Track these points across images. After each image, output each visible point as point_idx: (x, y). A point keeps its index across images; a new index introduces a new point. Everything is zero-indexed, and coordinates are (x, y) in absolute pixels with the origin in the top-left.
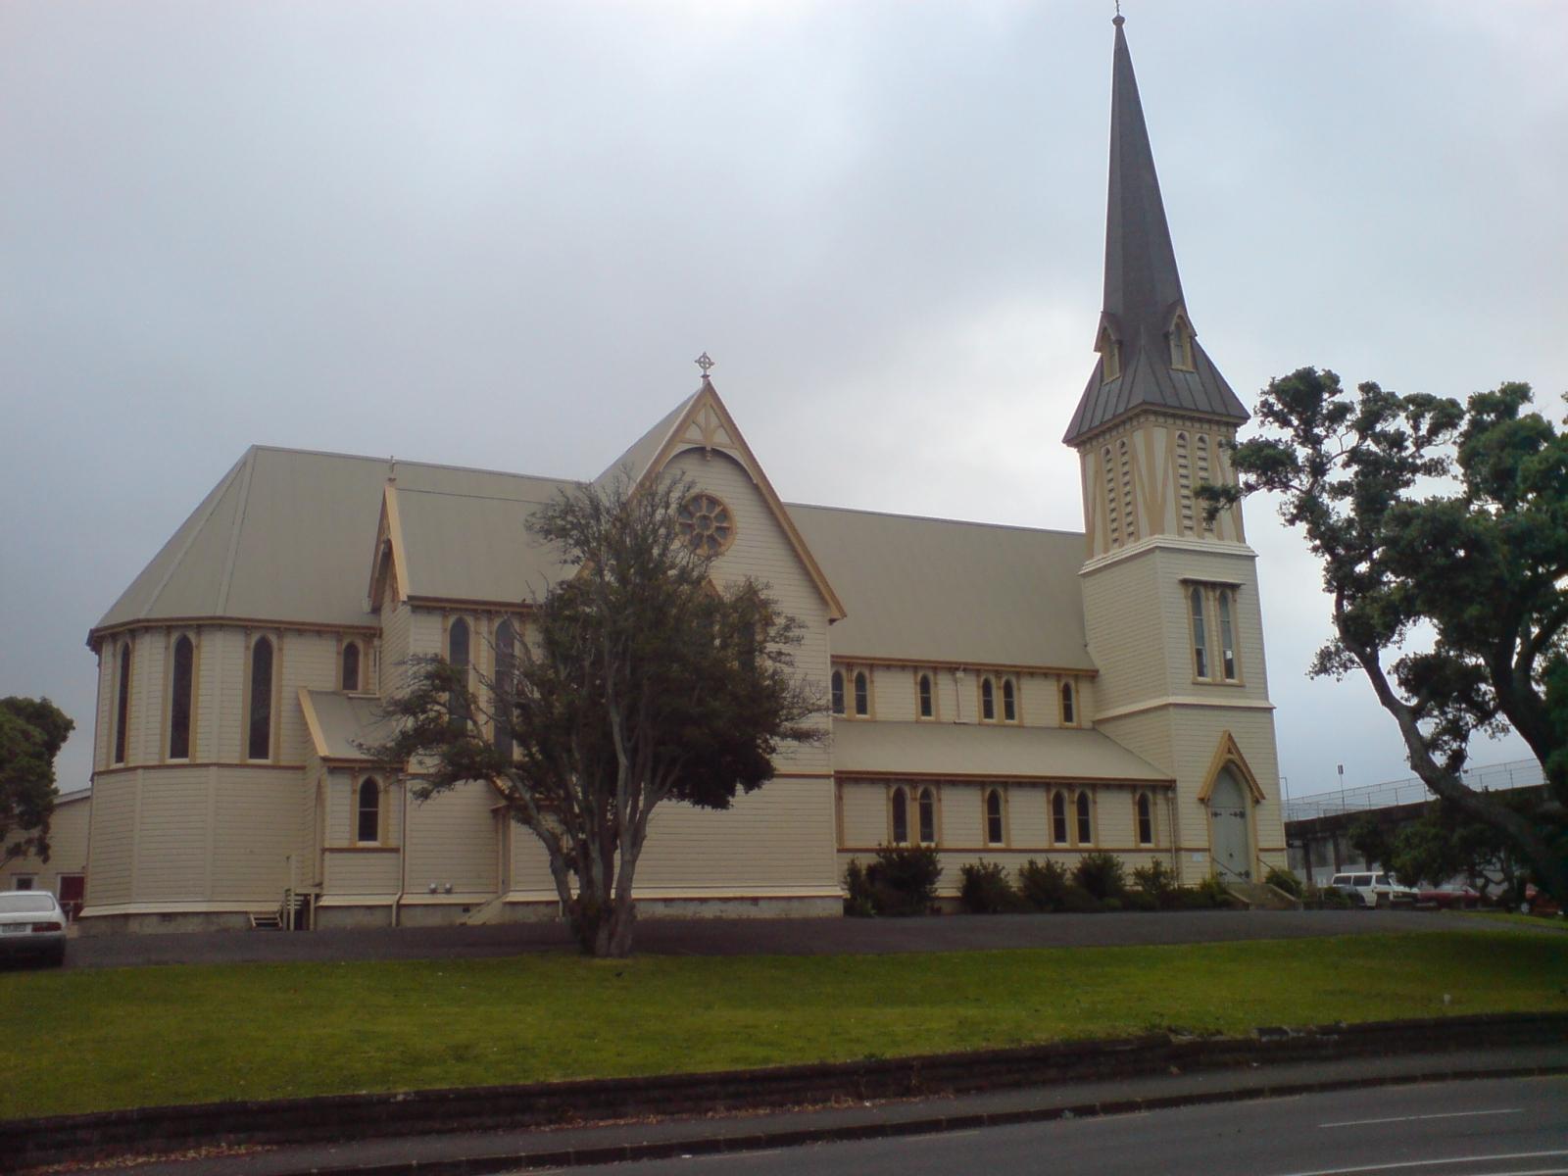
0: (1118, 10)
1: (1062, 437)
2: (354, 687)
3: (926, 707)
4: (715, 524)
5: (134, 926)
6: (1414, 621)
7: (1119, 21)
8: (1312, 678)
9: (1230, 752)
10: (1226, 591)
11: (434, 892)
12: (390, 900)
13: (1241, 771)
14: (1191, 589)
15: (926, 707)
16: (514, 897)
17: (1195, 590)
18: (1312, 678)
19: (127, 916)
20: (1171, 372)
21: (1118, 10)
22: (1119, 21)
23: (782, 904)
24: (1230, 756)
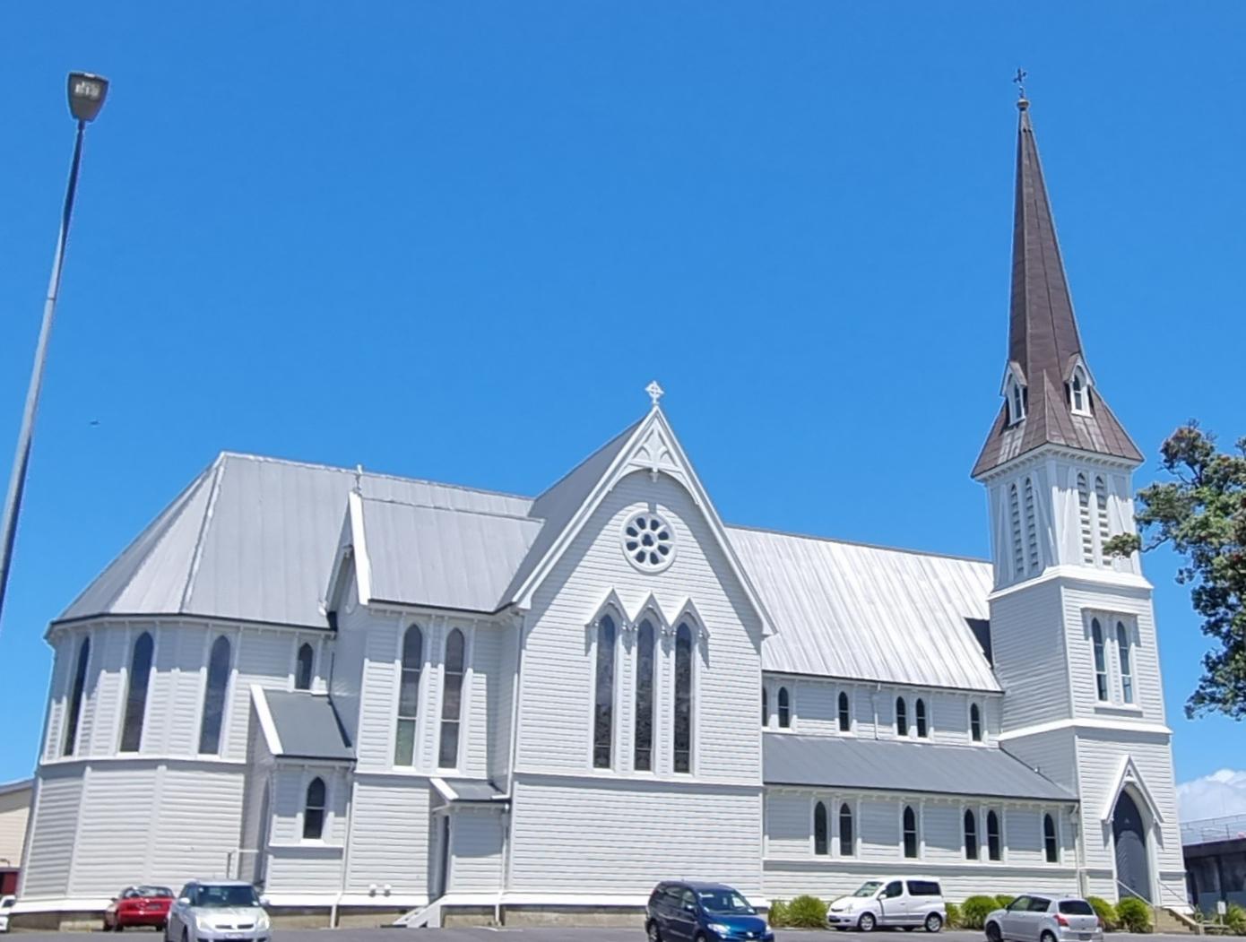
2: (136, 748)
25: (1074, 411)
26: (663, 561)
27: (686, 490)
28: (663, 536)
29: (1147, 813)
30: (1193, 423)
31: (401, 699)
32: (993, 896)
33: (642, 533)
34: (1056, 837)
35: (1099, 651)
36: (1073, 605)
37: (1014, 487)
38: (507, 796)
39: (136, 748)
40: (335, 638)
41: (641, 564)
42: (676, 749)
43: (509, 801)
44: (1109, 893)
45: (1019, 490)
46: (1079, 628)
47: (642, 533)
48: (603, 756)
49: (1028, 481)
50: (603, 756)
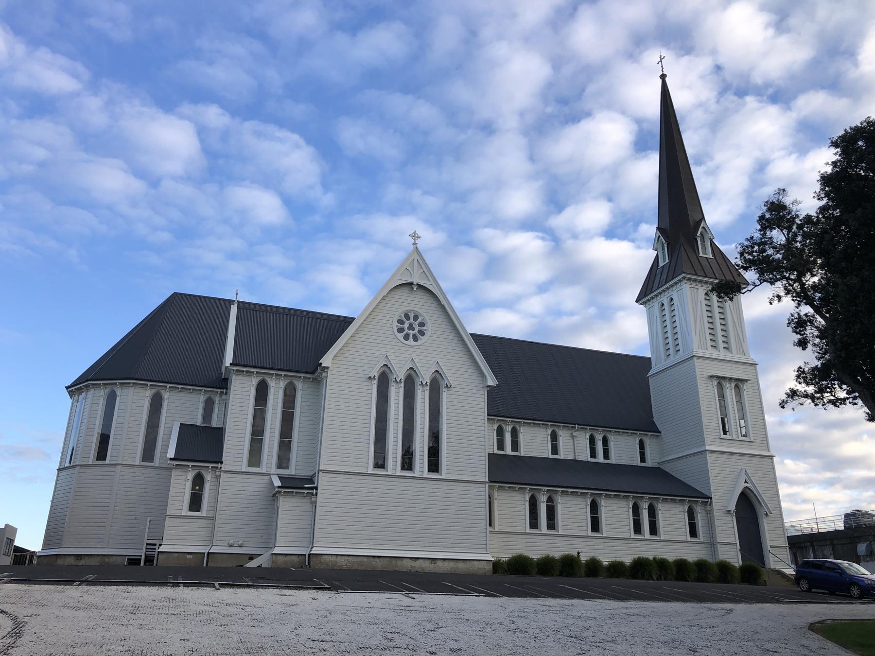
0: (663, 72)
1: (635, 300)
2: (258, 464)
3: (596, 526)
4: (406, 331)
5: (60, 562)
6: (868, 413)
7: (663, 77)
8: (830, 139)
9: (746, 482)
10: (739, 383)
11: (230, 546)
12: (205, 550)
13: (755, 495)
14: (715, 383)
15: (596, 526)
16: (277, 550)
17: (719, 383)
18: (830, 139)
19: (57, 556)
20: (699, 258)
21: (663, 72)
22: (663, 77)
23: (452, 564)
24: (746, 485)
25: (701, 255)
26: (421, 339)
27: (437, 297)
28: (416, 318)
29: (758, 504)
30: (819, 172)
31: (254, 425)
32: (651, 557)
33: (417, 328)
34: (645, 451)
35: (722, 396)
36: (703, 370)
37: (663, 305)
38: (315, 485)
39: (258, 464)
40: (226, 393)
41: (407, 342)
42: (429, 457)
43: (316, 488)
44: (733, 556)
45: (666, 306)
46: (704, 408)
47: (417, 328)
48: (380, 464)
49: (672, 299)
50: (380, 464)
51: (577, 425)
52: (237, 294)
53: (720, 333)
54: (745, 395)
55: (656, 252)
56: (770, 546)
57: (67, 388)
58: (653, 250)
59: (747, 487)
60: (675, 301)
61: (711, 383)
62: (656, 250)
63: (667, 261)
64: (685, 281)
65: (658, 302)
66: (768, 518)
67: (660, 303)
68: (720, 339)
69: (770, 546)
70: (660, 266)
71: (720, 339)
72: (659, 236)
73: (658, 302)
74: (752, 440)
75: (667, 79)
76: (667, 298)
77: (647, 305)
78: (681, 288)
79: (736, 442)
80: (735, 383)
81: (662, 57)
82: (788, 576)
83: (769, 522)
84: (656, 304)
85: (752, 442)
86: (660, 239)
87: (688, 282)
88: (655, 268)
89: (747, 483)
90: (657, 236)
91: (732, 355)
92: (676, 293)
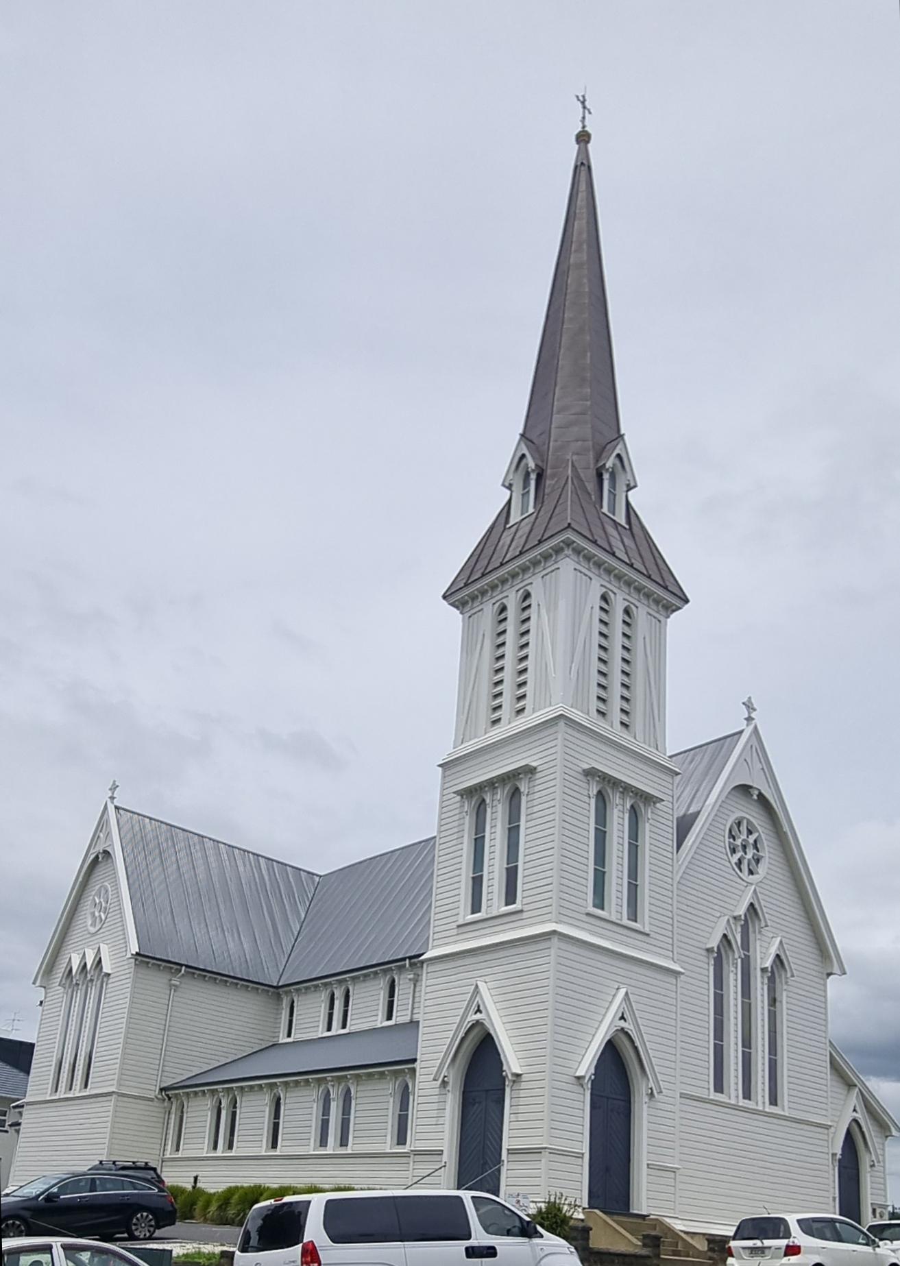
7: (583, 138)
13: (636, 1049)
22: (583, 138)
24: (622, 1024)
25: (605, 510)
45: (511, 613)
51: (184, 968)
52: (539, 605)
53: (617, 691)
54: (647, 832)
55: (508, 492)
56: (648, 1165)
57: (445, 597)
58: (503, 485)
59: (622, 1029)
60: (533, 601)
61: (585, 785)
62: (510, 487)
63: (531, 510)
64: (568, 552)
65: (493, 601)
66: (652, 1104)
67: (522, 591)
68: (616, 704)
69: (648, 1165)
70: (512, 523)
71: (616, 704)
72: (523, 456)
73: (493, 601)
74: (647, 930)
75: (591, 147)
76: (517, 591)
77: (467, 608)
78: (556, 566)
79: (615, 928)
80: (632, 801)
81: (581, 99)
82: (678, 1234)
83: (653, 1111)
84: (488, 610)
85: (648, 935)
86: (524, 461)
87: (574, 557)
88: (499, 528)
89: (625, 1020)
90: (519, 455)
91: (657, 753)
92: (540, 579)
